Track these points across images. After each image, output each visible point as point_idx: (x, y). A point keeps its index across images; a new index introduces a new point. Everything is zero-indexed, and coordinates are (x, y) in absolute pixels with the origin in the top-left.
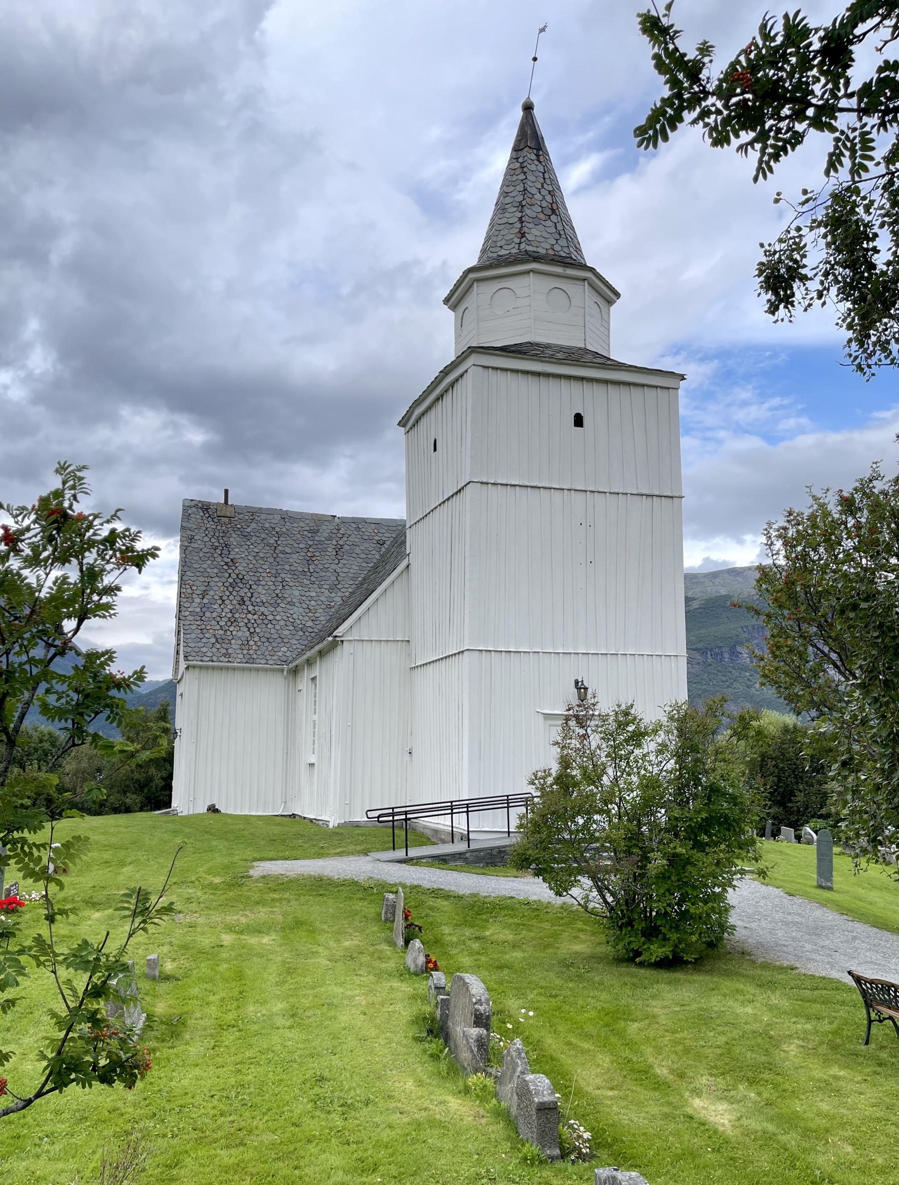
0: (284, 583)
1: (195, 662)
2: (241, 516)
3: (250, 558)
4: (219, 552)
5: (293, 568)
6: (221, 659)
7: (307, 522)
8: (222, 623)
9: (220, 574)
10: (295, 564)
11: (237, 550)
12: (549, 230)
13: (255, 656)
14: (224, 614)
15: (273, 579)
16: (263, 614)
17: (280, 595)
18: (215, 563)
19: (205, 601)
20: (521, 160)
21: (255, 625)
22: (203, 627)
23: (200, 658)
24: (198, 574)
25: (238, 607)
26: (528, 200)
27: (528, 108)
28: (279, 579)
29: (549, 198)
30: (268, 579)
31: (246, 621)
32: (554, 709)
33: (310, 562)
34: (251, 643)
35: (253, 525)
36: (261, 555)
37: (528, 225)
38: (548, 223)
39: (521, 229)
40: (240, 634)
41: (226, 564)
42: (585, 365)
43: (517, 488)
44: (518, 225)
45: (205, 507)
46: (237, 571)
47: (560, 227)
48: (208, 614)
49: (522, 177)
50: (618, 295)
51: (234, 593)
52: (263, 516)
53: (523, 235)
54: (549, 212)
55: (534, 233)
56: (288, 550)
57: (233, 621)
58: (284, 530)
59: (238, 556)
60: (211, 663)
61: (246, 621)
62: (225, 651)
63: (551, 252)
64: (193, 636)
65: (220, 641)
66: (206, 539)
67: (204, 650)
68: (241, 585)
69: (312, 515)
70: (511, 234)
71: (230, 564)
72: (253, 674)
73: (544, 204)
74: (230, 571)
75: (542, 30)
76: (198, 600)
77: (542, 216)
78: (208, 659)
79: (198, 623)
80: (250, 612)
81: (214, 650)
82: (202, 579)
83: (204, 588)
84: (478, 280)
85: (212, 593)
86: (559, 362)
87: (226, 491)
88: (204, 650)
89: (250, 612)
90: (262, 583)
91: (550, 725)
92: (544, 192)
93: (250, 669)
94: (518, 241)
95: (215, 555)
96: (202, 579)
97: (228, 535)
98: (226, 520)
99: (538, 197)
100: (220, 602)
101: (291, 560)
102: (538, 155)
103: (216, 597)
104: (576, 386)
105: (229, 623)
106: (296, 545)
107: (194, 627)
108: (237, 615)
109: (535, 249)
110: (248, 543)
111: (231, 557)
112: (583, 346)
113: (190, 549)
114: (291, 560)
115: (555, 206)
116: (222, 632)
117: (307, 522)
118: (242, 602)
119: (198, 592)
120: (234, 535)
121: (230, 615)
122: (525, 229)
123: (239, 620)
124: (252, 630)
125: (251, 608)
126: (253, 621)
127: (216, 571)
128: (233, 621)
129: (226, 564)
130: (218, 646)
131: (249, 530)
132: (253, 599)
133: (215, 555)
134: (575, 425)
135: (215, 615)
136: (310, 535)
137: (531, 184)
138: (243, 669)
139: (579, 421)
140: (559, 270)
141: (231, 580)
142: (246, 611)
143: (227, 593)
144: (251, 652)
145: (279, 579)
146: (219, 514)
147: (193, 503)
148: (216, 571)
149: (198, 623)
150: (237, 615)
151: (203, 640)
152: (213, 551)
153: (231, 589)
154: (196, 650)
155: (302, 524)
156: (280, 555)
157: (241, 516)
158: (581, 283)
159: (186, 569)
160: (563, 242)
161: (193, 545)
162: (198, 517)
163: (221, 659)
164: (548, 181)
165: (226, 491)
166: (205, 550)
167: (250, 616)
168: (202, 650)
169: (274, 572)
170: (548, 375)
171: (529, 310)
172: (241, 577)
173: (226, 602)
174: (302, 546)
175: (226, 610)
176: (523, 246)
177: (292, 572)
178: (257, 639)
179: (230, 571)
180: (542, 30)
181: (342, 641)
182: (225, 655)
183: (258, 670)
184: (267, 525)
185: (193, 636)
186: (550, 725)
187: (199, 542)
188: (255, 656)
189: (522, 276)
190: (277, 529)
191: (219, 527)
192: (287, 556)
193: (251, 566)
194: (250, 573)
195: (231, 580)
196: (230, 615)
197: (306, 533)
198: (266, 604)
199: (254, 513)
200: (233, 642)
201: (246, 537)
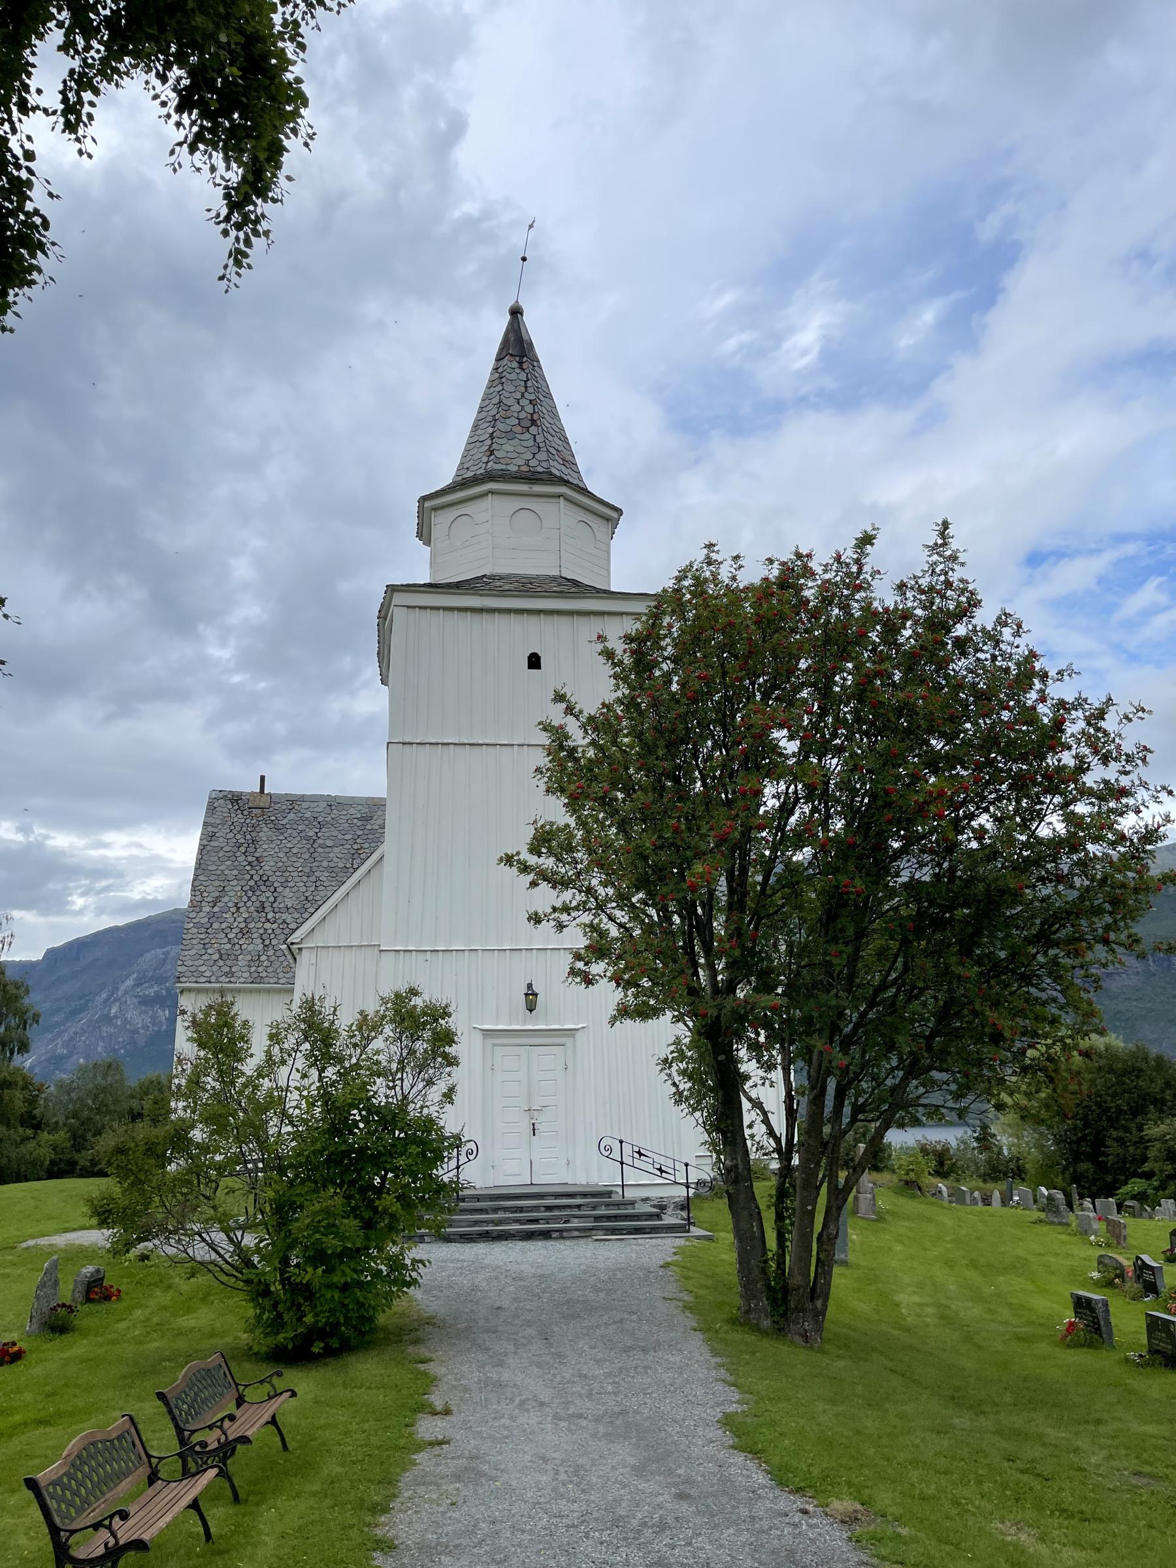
0: (318, 883)
1: (188, 985)
2: (277, 807)
3: (281, 855)
4: (243, 849)
5: (332, 864)
6: (221, 979)
7: (360, 807)
8: (231, 936)
9: (240, 877)
10: (336, 860)
11: (265, 846)
12: (524, 443)
13: (264, 974)
14: (235, 924)
15: (305, 879)
16: (284, 922)
17: (310, 898)
18: (236, 863)
19: (216, 909)
20: (500, 370)
21: (272, 936)
22: (207, 941)
23: (194, 979)
24: (213, 877)
25: (255, 914)
26: (502, 413)
27: (516, 312)
28: (313, 879)
29: (529, 409)
30: (298, 879)
31: (262, 931)
32: (525, 1023)
33: (356, 856)
34: (263, 958)
35: (291, 816)
36: (295, 851)
37: (499, 441)
38: (527, 436)
39: (490, 446)
40: (251, 947)
41: (250, 863)
42: (536, 595)
43: (452, 747)
44: (489, 442)
45: (235, 799)
46: (261, 872)
47: (539, 439)
48: (216, 925)
49: (499, 388)
50: (619, 511)
51: (254, 898)
52: (305, 805)
53: (492, 453)
54: (527, 423)
55: (506, 448)
56: (329, 843)
57: (244, 932)
58: (329, 819)
59: (265, 854)
60: (207, 985)
61: (262, 931)
62: (227, 969)
63: (525, 469)
64: (192, 952)
65: (224, 957)
66: (231, 835)
67: (203, 968)
68: (263, 888)
69: (367, 799)
70: (480, 453)
71: (255, 863)
72: (263, 996)
73: (522, 415)
74: (253, 872)
75: (531, 226)
76: (207, 909)
77: (518, 429)
78: (204, 979)
79: (202, 936)
80: (268, 920)
81: (215, 968)
82: (217, 883)
83: (217, 894)
84: (435, 509)
85: (226, 899)
86: (503, 593)
87: (263, 778)
88: (203, 968)
89: (268, 920)
90: (290, 884)
91: (494, 1045)
92: (523, 402)
93: (259, 991)
94: (485, 459)
95: (238, 854)
96: (217, 883)
97: (258, 829)
98: (259, 811)
99: (517, 408)
100: (233, 910)
101: (331, 855)
102: (521, 363)
103: (230, 904)
104: (532, 621)
105: (240, 935)
106: (340, 836)
107: (195, 942)
108: (251, 925)
109: (504, 467)
110: (282, 837)
111: (257, 855)
112: (556, 573)
113: (208, 848)
114: (331, 855)
115: (536, 417)
116: (229, 946)
117: (360, 807)
118: (262, 908)
119: (210, 899)
120: (265, 829)
121: (243, 925)
122: (494, 446)
123: (254, 930)
124: (267, 942)
125: (270, 916)
126: (270, 931)
127: (235, 872)
128: (244, 932)
129: (250, 863)
130: (221, 963)
131: (284, 822)
132: (275, 905)
133: (238, 854)
134: (539, 668)
135: (224, 925)
136: (360, 823)
137: (507, 395)
138: (250, 991)
139: (534, 662)
140: (524, 488)
141: (252, 883)
142: (263, 920)
143: (245, 899)
144: (260, 969)
145: (313, 879)
146: (251, 805)
147: (221, 795)
148: (235, 872)
149: (202, 936)
150: (251, 925)
151: (204, 957)
152: (235, 849)
153: (250, 894)
154: (193, 969)
155: (352, 811)
156: (320, 850)
157: (277, 807)
158: (556, 500)
159: (200, 872)
160: (542, 456)
161: (213, 844)
162: (225, 810)
163: (221, 979)
164: (531, 390)
165: (263, 778)
166: (227, 849)
167: (267, 925)
168: (201, 969)
169: (307, 870)
170: (481, 610)
171: (510, 537)
172: (265, 878)
173: (241, 910)
174: (348, 837)
175: (240, 919)
176: (490, 464)
177: (331, 870)
178: (271, 953)
179: (253, 872)
180: (531, 226)
181: (300, 949)
182: (226, 974)
183: (268, 991)
184: (308, 815)
185: (192, 952)
186: (494, 1045)
187: (221, 839)
188: (264, 974)
189: (480, 500)
190: (320, 819)
191: (248, 821)
192: (328, 850)
193: (280, 864)
194: (278, 874)
195: (252, 883)
196: (243, 925)
197: (355, 821)
198: (291, 910)
199: (294, 802)
200: (240, 957)
201: (280, 829)
